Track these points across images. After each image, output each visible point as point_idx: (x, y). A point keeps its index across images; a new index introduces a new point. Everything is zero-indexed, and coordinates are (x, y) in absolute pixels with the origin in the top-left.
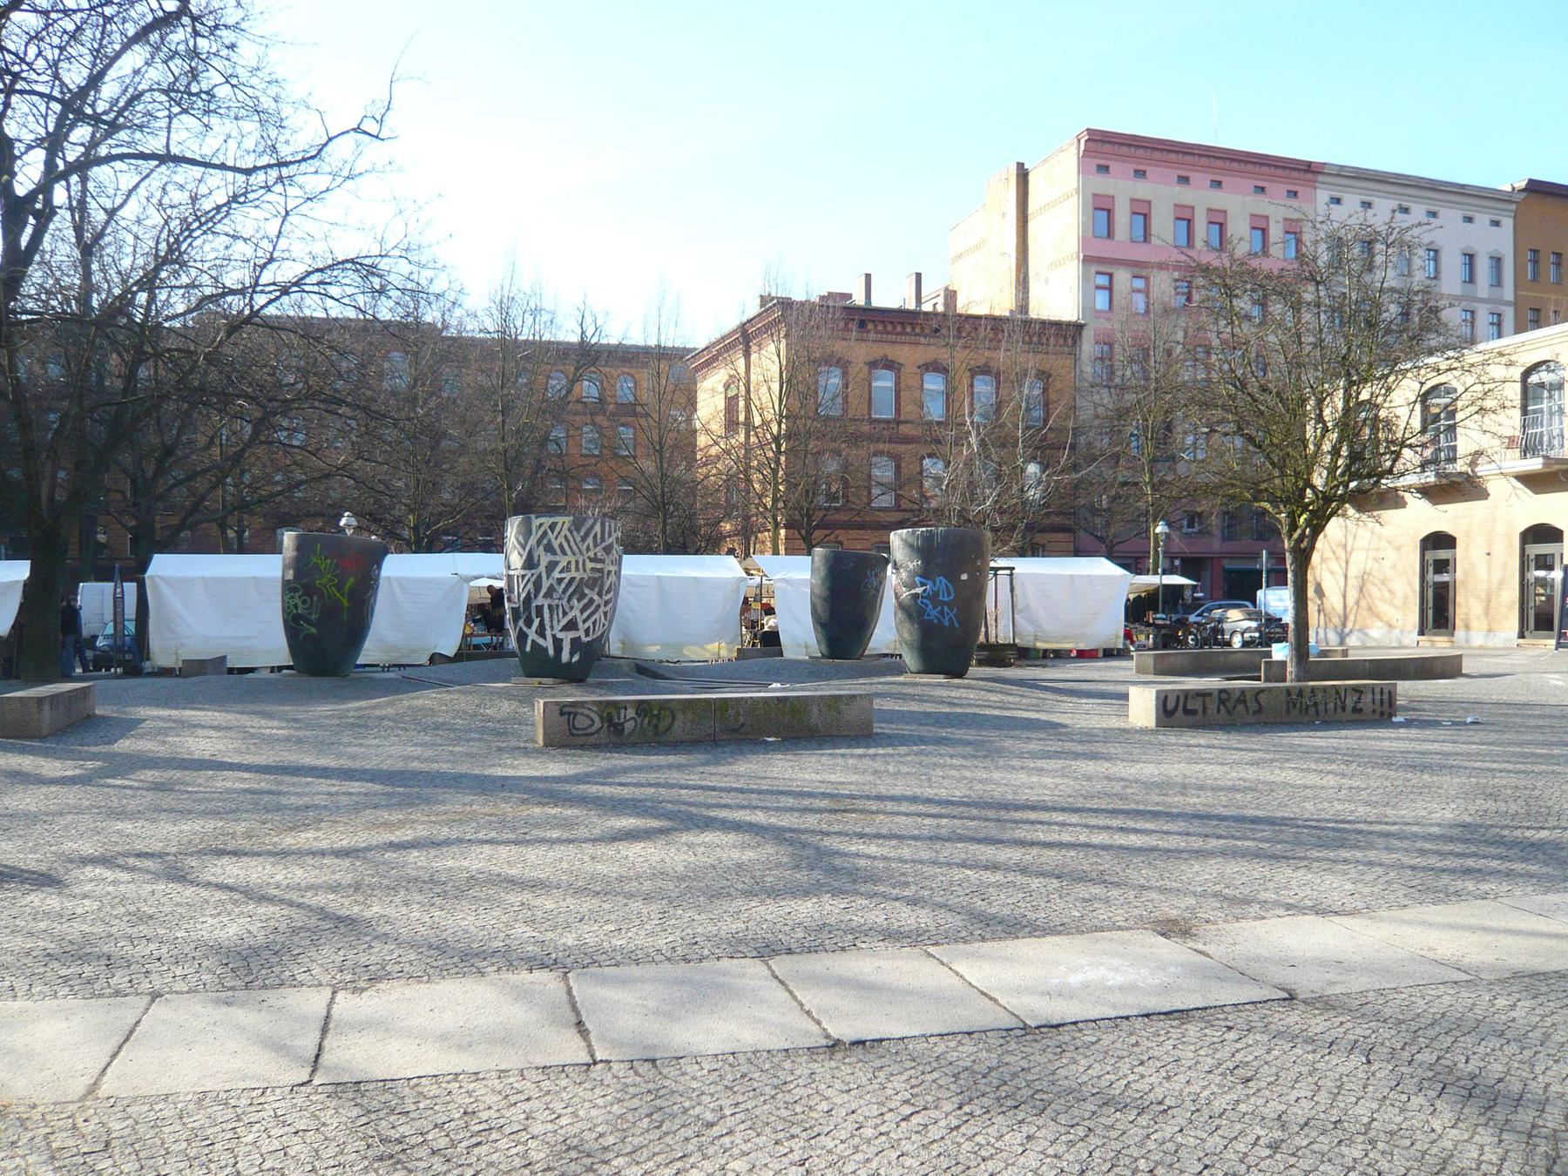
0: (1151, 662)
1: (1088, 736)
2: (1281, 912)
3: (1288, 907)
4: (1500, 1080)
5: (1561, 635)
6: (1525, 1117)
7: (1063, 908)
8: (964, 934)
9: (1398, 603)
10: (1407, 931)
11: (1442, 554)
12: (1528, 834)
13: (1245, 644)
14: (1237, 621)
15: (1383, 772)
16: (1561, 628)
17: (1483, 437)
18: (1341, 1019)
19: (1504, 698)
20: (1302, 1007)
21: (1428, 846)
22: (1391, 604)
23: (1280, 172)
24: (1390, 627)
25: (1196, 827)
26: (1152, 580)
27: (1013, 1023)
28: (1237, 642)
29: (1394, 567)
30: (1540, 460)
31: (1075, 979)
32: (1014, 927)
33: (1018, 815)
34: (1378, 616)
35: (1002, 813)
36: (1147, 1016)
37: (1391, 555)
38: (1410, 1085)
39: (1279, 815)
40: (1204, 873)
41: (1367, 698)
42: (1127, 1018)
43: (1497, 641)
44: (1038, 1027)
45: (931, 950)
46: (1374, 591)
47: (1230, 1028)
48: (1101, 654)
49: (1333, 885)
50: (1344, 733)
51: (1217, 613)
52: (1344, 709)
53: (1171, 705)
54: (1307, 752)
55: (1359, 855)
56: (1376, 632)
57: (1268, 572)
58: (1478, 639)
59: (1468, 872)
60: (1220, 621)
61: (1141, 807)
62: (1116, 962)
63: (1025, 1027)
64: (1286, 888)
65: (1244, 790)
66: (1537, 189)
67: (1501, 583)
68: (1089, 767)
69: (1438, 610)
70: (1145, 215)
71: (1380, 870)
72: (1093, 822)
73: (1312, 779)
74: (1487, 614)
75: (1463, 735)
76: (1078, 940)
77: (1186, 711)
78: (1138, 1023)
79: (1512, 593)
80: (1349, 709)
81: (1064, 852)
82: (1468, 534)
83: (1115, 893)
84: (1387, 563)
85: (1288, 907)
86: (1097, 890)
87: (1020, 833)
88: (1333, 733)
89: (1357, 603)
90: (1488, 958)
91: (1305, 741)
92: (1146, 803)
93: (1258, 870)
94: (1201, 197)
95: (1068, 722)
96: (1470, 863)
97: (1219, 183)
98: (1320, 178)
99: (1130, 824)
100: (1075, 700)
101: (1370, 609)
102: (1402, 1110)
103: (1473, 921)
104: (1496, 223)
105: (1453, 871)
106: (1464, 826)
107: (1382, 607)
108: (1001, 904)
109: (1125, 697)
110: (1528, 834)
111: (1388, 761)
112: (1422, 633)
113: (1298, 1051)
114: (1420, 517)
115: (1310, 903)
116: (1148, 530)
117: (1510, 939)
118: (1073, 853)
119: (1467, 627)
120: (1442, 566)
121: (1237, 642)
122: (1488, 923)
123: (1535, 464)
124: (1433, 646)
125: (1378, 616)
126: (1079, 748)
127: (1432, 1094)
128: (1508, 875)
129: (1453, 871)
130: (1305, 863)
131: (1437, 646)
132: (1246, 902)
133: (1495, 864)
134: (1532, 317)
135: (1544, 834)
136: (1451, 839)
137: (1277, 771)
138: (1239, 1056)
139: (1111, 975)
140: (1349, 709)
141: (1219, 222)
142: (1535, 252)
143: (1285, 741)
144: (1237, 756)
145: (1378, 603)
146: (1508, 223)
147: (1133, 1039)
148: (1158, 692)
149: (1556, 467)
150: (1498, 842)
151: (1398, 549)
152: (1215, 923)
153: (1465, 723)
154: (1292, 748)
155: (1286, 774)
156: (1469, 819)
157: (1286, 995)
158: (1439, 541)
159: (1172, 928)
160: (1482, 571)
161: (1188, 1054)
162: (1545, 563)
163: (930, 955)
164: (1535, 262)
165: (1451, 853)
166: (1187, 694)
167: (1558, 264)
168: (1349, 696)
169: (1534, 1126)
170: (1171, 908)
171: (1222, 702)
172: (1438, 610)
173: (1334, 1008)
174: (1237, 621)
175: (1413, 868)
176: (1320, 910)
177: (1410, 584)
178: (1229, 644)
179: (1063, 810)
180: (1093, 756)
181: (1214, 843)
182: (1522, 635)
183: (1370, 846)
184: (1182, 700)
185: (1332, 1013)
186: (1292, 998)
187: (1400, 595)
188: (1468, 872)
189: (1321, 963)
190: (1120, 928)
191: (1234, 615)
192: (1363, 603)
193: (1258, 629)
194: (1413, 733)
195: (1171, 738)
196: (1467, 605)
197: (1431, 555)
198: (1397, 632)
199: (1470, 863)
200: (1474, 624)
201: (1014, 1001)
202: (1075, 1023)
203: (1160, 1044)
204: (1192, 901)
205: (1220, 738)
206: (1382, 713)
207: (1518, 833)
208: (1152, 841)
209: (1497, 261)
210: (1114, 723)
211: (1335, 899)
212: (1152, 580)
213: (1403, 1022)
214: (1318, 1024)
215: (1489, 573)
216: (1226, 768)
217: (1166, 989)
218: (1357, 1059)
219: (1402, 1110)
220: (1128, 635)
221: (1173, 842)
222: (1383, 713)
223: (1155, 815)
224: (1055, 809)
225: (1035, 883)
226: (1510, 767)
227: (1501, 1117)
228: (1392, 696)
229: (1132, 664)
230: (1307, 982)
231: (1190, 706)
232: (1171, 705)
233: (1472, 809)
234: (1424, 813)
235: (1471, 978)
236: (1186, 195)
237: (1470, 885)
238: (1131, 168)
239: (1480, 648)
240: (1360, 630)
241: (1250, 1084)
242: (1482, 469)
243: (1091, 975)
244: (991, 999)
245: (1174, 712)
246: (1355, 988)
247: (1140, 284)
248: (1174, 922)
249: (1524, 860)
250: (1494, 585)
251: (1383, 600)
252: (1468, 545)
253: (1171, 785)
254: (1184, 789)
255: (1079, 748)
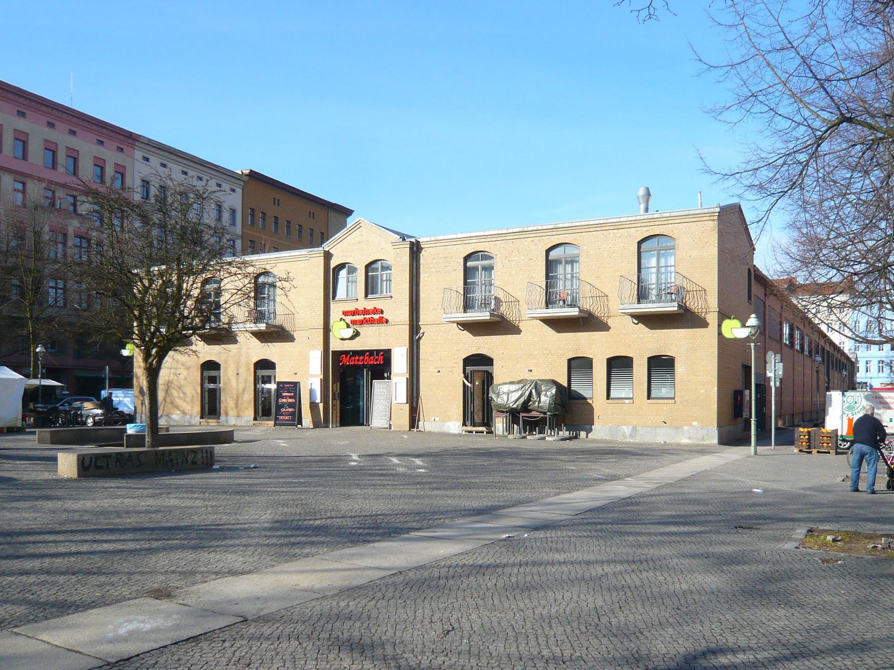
0: (48, 436)
1: (35, 485)
2: (214, 577)
3: (216, 573)
4: (361, 639)
5: (276, 419)
6: (379, 652)
7: (87, 590)
8: (32, 617)
9: (188, 399)
10: (282, 577)
11: (213, 373)
12: (311, 522)
13: (95, 423)
14: (92, 411)
15: (224, 496)
16: (276, 414)
17: (236, 310)
18: (276, 626)
19: (262, 453)
20: (254, 624)
21: (268, 534)
22: (185, 401)
23: (113, 134)
24: (182, 413)
25: (138, 535)
26: (35, 382)
27: (101, 663)
28: (90, 421)
29: (185, 379)
30: (265, 325)
31: (122, 631)
32: (64, 608)
33: (21, 539)
34: (177, 408)
35: (9, 538)
36: (176, 643)
37: (184, 373)
38: (324, 650)
39: (182, 524)
40: (161, 561)
41: (199, 455)
42: (166, 647)
43: (242, 422)
44: (117, 662)
45: (15, 630)
46: (175, 393)
47: (224, 641)
48: (5, 431)
49: (233, 559)
50: (191, 476)
51: (77, 404)
52: (187, 462)
53: (87, 464)
54: (178, 488)
55: (237, 542)
56: (176, 416)
57: (109, 379)
58: (232, 421)
59: (294, 544)
60: (80, 408)
61: (99, 527)
62: (140, 618)
63: (109, 664)
64: (209, 564)
65: (155, 512)
66: (254, 176)
67: (244, 390)
68: (49, 504)
69: (211, 404)
70: (24, 142)
71: (252, 548)
72: (74, 538)
73: (189, 503)
74: (237, 406)
75: (253, 474)
76: (109, 609)
77: (98, 467)
78: (174, 649)
79: (249, 396)
80: (189, 462)
81: (67, 559)
82: (226, 362)
83: (114, 579)
84: (182, 377)
85: (216, 573)
86: (102, 579)
87: (30, 550)
88: (185, 476)
89: (165, 399)
90: (324, 584)
91: (172, 482)
92: (99, 523)
93: (190, 555)
94: (62, 138)
95: (15, 476)
96: (292, 540)
97: (122, 150)
98: (137, 144)
99: (98, 537)
100: (11, 462)
101: (172, 403)
102: (328, 662)
103: (308, 568)
104: (233, 190)
105: (287, 545)
106: (277, 522)
107: (180, 402)
108: (46, 594)
109: (55, 459)
110: (311, 522)
111: (224, 490)
112: (202, 417)
113: (265, 645)
114: (205, 351)
115: (226, 570)
116: (29, 348)
117: (330, 575)
118: (73, 559)
119: (227, 414)
120: (214, 380)
121: (90, 421)
122: (316, 568)
123: (262, 327)
124: (208, 425)
125: (177, 408)
126: (35, 493)
127: (337, 652)
128: (312, 543)
129: (287, 545)
130: (212, 549)
131: (211, 425)
132: (193, 573)
133: (304, 539)
134: (255, 248)
135: (318, 522)
136: (277, 529)
137: (167, 500)
138: (237, 654)
139: (142, 625)
140: (189, 462)
141: (74, 157)
142: (253, 210)
143: (161, 482)
144: (139, 492)
145: (177, 400)
146: (239, 191)
147: (176, 657)
148: (78, 456)
149: (272, 329)
150: (299, 528)
151: (188, 369)
152: (181, 588)
153: (250, 468)
154: (168, 486)
155: (172, 501)
156: (280, 518)
157: (242, 619)
158: (210, 366)
159: (160, 594)
160: (234, 383)
161: (209, 657)
162: (267, 380)
163: (17, 634)
164: (253, 215)
165: (281, 536)
166: (97, 456)
167: (264, 219)
168: (186, 456)
169: (384, 656)
170: (156, 582)
171: (118, 460)
172: (211, 404)
173: (269, 621)
174: (92, 411)
175: (267, 545)
176: (233, 573)
177: (195, 389)
178: (85, 423)
179: (50, 533)
180: (48, 498)
181: (155, 544)
182: (255, 419)
183: (239, 537)
184: (94, 460)
185: (270, 624)
186: (246, 620)
187: (189, 395)
188: (294, 544)
189: (249, 599)
190: (129, 599)
191: (88, 405)
192: (168, 400)
193: (102, 415)
194: (227, 474)
195: (86, 484)
196: (227, 402)
197: (207, 373)
198: (188, 417)
199: (292, 540)
200: (230, 413)
201: (94, 650)
202: (138, 655)
203: (192, 656)
204: (162, 578)
205: (122, 483)
206: (207, 464)
207: (306, 522)
208: (119, 546)
209: (233, 211)
210: (47, 476)
211: (238, 566)
212: (35, 382)
213: (305, 622)
214: (266, 630)
215: (238, 385)
216: (136, 500)
217: (177, 627)
218: (294, 643)
219: (328, 662)
220: (24, 419)
221: (132, 546)
222: (206, 463)
223: (112, 531)
224: (44, 533)
225: (61, 579)
226: (285, 489)
227: (369, 655)
228: (212, 453)
229: (36, 437)
230: (250, 610)
231: (99, 464)
232: (87, 464)
233: (279, 513)
234: (257, 517)
235: (322, 595)
236: (53, 135)
237: (298, 551)
238: (15, 109)
239: (234, 425)
240: (167, 415)
241: (251, 666)
242: (234, 328)
243: (131, 627)
244: (76, 652)
245: (89, 468)
246: (273, 610)
247: (49, 194)
248: (159, 590)
249: (316, 536)
250: (240, 391)
251: (179, 398)
252: (226, 368)
253: (110, 513)
254: (118, 514)
255: (35, 493)
